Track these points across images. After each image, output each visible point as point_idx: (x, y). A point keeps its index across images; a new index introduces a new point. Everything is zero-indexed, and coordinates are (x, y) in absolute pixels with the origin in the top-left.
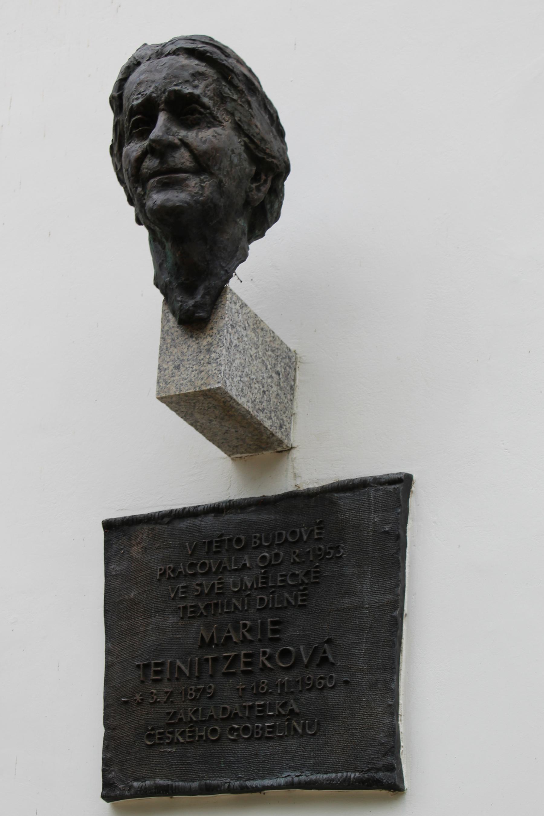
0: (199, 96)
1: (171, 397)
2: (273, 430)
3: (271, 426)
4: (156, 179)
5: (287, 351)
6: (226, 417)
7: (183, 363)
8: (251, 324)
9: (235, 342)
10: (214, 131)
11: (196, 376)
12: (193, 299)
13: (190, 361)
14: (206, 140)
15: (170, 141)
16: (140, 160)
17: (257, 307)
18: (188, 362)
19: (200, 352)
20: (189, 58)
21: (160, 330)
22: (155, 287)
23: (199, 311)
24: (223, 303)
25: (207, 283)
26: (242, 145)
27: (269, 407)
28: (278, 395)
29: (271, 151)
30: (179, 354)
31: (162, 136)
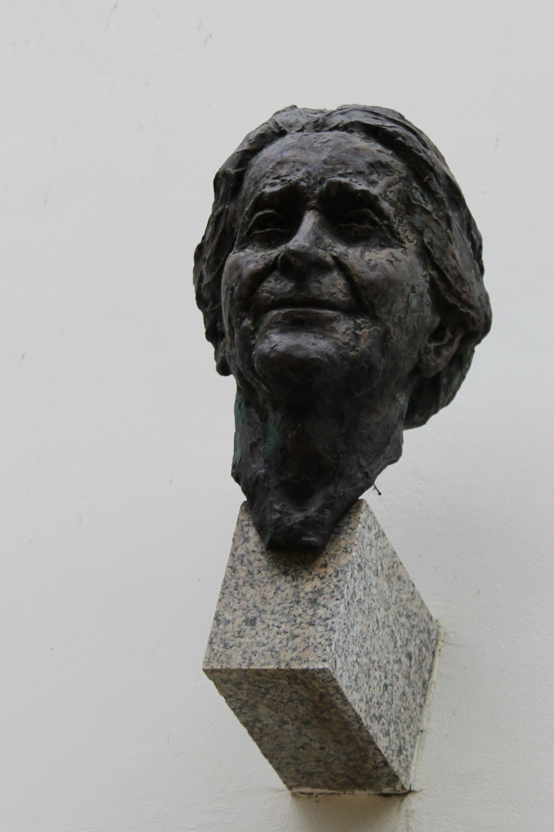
0: (376, 198)
1: (230, 672)
2: (388, 755)
3: (387, 748)
4: (283, 311)
5: (427, 620)
6: (314, 722)
7: (263, 615)
8: (385, 567)
9: (360, 594)
10: (391, 253)
11: (285, 643)
12: (301, 510)
13: (277, 616)
14: (376, 265)
15: (319, 258)
16: (260, 277)
17: (394, 538)
18: (273, 617)
19: (298, 602)
20: (368, 139)
21: (229, 553)
22: (232, 480)
23: (310, 533)
24: (351, 525)
25: (331, 489)
26: (426, 281)
27: (389, 713)
28: (404, 694)
29: (469, 297)
30: (258, 599)
31: (310, 248)
